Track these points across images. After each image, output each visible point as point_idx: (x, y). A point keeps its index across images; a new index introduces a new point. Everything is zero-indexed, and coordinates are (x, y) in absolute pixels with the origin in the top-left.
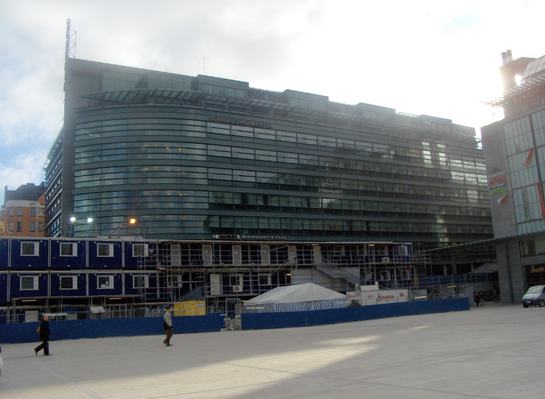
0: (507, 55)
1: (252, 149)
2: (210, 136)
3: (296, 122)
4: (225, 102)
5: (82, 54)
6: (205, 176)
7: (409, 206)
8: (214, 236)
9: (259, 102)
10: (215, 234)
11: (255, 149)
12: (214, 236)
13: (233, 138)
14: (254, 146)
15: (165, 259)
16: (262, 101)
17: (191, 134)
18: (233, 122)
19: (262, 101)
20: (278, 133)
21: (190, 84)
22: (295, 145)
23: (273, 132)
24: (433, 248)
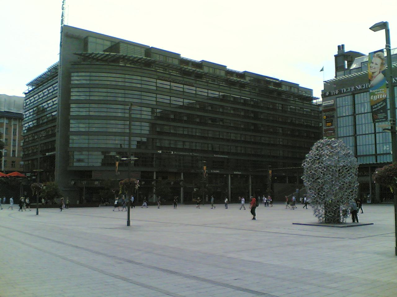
0: (341, 48)
1: (169, 96)
2: (159, 89)
3: (208, 83)
4: (167, 66)
5: (70, 22)
6: (154, 84)
7: (218, 133)
8: (159, 152)
9: (187, 68)
10: (159, 150)
11: (170, 96)
12: (159, 152)
13: (185, 94)
14: (170, 94)
15: (321, 196)
16: (118, 54)
17: (83, 74)
18: (172, 81)
19: (118, 54)
20: (198, 89)
21: (144, 52)
22: (168, 91)
23: (194, 88)
24: (276, 168)
